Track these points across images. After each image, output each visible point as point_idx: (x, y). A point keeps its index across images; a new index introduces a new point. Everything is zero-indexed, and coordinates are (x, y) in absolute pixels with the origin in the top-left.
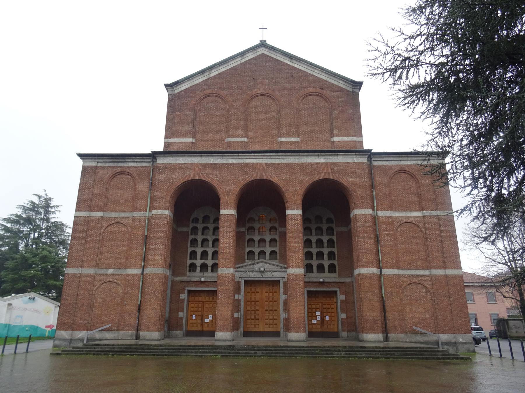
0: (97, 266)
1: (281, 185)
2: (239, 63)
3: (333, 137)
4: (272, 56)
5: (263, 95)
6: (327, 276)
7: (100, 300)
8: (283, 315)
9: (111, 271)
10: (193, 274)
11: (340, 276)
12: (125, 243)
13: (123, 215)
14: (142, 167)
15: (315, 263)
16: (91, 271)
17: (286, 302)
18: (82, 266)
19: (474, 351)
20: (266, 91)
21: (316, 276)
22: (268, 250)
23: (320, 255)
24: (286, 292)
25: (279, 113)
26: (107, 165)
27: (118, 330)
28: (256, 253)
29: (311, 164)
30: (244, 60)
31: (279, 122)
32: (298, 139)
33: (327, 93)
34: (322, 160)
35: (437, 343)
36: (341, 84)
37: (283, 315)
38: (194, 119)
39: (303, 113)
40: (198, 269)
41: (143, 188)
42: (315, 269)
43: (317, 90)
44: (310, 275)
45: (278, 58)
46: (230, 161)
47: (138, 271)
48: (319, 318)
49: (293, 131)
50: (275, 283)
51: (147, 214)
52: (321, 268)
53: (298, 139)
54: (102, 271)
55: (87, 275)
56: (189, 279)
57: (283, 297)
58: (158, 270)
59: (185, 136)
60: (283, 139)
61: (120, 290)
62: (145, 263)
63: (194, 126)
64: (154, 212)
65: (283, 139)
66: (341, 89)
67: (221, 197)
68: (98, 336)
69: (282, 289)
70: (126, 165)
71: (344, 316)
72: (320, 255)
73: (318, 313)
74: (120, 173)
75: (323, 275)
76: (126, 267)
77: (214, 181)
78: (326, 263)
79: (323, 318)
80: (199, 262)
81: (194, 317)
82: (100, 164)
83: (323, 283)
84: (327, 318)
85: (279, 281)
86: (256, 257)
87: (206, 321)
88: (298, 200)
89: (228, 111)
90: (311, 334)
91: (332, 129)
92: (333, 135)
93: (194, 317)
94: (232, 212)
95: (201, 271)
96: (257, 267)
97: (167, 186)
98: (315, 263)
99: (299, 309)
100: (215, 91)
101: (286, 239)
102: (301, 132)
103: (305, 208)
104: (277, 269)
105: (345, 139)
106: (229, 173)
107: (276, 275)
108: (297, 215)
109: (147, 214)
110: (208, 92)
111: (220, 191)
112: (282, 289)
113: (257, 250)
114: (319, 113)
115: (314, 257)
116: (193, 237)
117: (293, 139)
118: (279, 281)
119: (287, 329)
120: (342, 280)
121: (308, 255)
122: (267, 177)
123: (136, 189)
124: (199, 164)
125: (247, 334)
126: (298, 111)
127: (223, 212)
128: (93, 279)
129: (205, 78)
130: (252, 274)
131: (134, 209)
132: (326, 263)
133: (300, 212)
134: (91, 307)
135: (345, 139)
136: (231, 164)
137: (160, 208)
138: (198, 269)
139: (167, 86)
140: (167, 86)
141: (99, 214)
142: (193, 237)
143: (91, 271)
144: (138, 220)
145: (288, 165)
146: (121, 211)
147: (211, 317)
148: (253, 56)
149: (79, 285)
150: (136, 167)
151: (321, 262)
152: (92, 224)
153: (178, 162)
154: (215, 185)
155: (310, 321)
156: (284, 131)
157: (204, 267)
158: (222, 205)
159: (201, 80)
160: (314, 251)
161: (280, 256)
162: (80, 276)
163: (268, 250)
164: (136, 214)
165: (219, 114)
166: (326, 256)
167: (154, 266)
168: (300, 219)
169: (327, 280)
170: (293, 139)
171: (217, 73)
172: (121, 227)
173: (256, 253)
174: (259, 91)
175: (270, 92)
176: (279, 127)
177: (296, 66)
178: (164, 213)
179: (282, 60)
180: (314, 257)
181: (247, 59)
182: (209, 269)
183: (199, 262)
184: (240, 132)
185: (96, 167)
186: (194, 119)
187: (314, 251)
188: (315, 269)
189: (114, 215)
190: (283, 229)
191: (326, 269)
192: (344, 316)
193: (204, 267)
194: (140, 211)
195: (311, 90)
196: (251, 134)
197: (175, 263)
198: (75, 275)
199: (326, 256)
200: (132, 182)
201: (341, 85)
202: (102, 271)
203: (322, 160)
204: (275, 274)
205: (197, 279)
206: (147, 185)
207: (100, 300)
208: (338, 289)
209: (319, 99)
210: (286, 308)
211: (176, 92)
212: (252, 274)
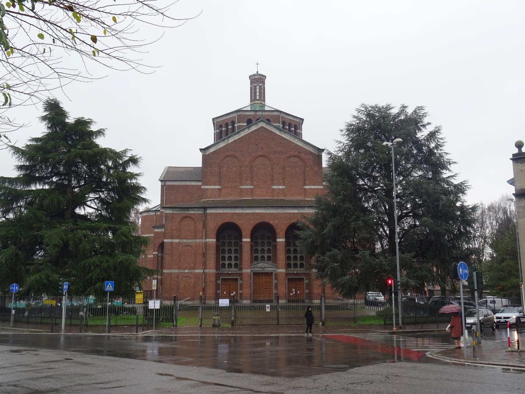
0: (179, 269)
1: (274, 225)
2: (247, 133)
3: (305, 185)
4: (268, 128)
5: (261, 156)
6: (299, 270)
7: (182, 286)
8: (275, 291)
9: (187, 271)
10: (225, 269)
11: (306, 270)
12: (193, 256)
13: (190, 241)
14: (198, 214)
15: (292, 262)
16: (177, 271)
17: (276, 284)
18: (172, 269)
19: (364, 308)
20: (264, 154)
21: (293, 270)
22: (266, 255)
23: (295, 258)
24: (276, 279)
25: (272, 169)
26: (178, 212)
27: (193, 300)
28: (259, 257)
29: (290, 213)
30: (250, 131)
31: (273, 175)
32: (284, 187)
33: (303, 155)
34: (296, 211)
35: (347, 304)
36: (311, 150)
37: (275, 291)
38: (220, 173)
39: (287, 169)
40: (227, 266)
41: (200, 226)
42: (292, 266)
43: (296, 153)
44: (289, 269)
45: (272, 130)
46: (247, 212)
47: (201, 271)
48: (294, 293)
49: (281, 181)
50: (270, 274)
51: (204, 241)
52: (295, 265)
53: (284, 187)
54: (182, 271)
55: (175, 273)
56: (222, 272)
57: (275, 282)
58: (211, 271)
59: (214, 184)
60: (275, 187)
61: (192, 281)
62: (205, 267)
63: (220, 178)
64: (208, 240)
65: (275, 187)
66: (311, 153)
67: (243, 231)
68: (184, 303)
69: (274, 278)
70: (189, 212)
71: (307, 291)
72: (295, 258)
73: (294, 290)
74: (186, 217)
75: (297, 269)
76: (195, 269)
77: (239, 223)
78: (299, 263)
79: (296, 292)
80: (227, 262)
81: (225, 293)
82: (174, 212)
83: (297, 273)
84: (298, 292)
85: (272, 273)
86: (259, 260)
87: (232, 295)
88: (283, 233)
89: (241, 167)
90: (289, 301)
91: (305, 180)
92: (305, 185)
93: (225, 293)
94: (249, 240)
95: (228, 268)
96: (260, 265)
97: (213, 226)
98: (292, 262)
99: (282, 290)
100: (232, 153)
101: (276, 256)
102: (286, 182)
103: (287, 237)
104: (271, 266)
105: (312, 187)
106: (247, 217)
107: (270, 270)
108: (282, 242)
109: (204, 241)
110: (228, 154)
111: (242, 229)
112: (274, 278)
113: (260, 255)
114: (297, 169)
115: (292, 259)
116: (223, 248)
117: (281, 187)
118: (272, 273)
119: (242, 298)
120: (307, 272)
121: (288, 258)
122: (267, 221)
123: (195, 226)
124: (230, 213)
125: (255, 301)
126: (284, 168)
127: (244, 240)
128: (178, 275)
129: (225, 144)
130: (257, 269)
131: (195, 238)
132: (299, 263)
133: (284, 240)
134: (179, 289)
135: (312, 187)
136: (248, 213)
137: (211, 238)
138: (227, 266)
139: (201, 150)
140: (201, 150)
141: (177, 241)
142: (223, 248)
143: (177, 271)
144: (198, 244)
145: (278, 214)
146: (189, 239)
147: (234, 293)
148: (256, 128)
149: (171, 278)
150: (195, 214)
151: (296, 262)
152: (174, 246)
153: (218, 212)
154: (239, 225)
155: (289, 294)
156: (275, 182)
157: (230, 265)
158: (243, 236)
159: (223, 145)
160: (292, 256)
161: (272, 259)
162: (171, 274)
163: (266, 255)
164: (197, 241)
165: (235, 169)
166: (298, 259)
167: (210, 268)
168: (284, 244)
169: (298, 272)
170: (281, 187)
171: (233, 140)
172: (190, 248)
173: (259, 257)
174: (260, 154)
175: (267, 154)
176: (273, 179)
177: (283, 136)
178: (212, 240)
179: (274, 131)
180: (292, 259)
181: (252, 130)
182: (233, 266)
183: (227, 262)
184: (249, 182)
185: (172, 214)
186: (220, 173)
187: (292, 256)
188: (292, 266)
189: (185, 241)
190: (275, 243)
191: (299, 266)
192: (307, 291)
193: (230, 265)
194: (199, 239)
195: (292, 153)
196: (255, 183)
197: (219, 266)
198: (169, 273)
199: (298, 259)
200: (193, 222)
201: (311, 150)
202: (182, 271)
203: (296, 211)
204: (270, 269)
205: (227, 272)
206: (202, 224)
207: (182, 286)
208: (304, 277)
209: (297, 159)
210: (276, 288)
211: (207, 153)
212: (257, 269)
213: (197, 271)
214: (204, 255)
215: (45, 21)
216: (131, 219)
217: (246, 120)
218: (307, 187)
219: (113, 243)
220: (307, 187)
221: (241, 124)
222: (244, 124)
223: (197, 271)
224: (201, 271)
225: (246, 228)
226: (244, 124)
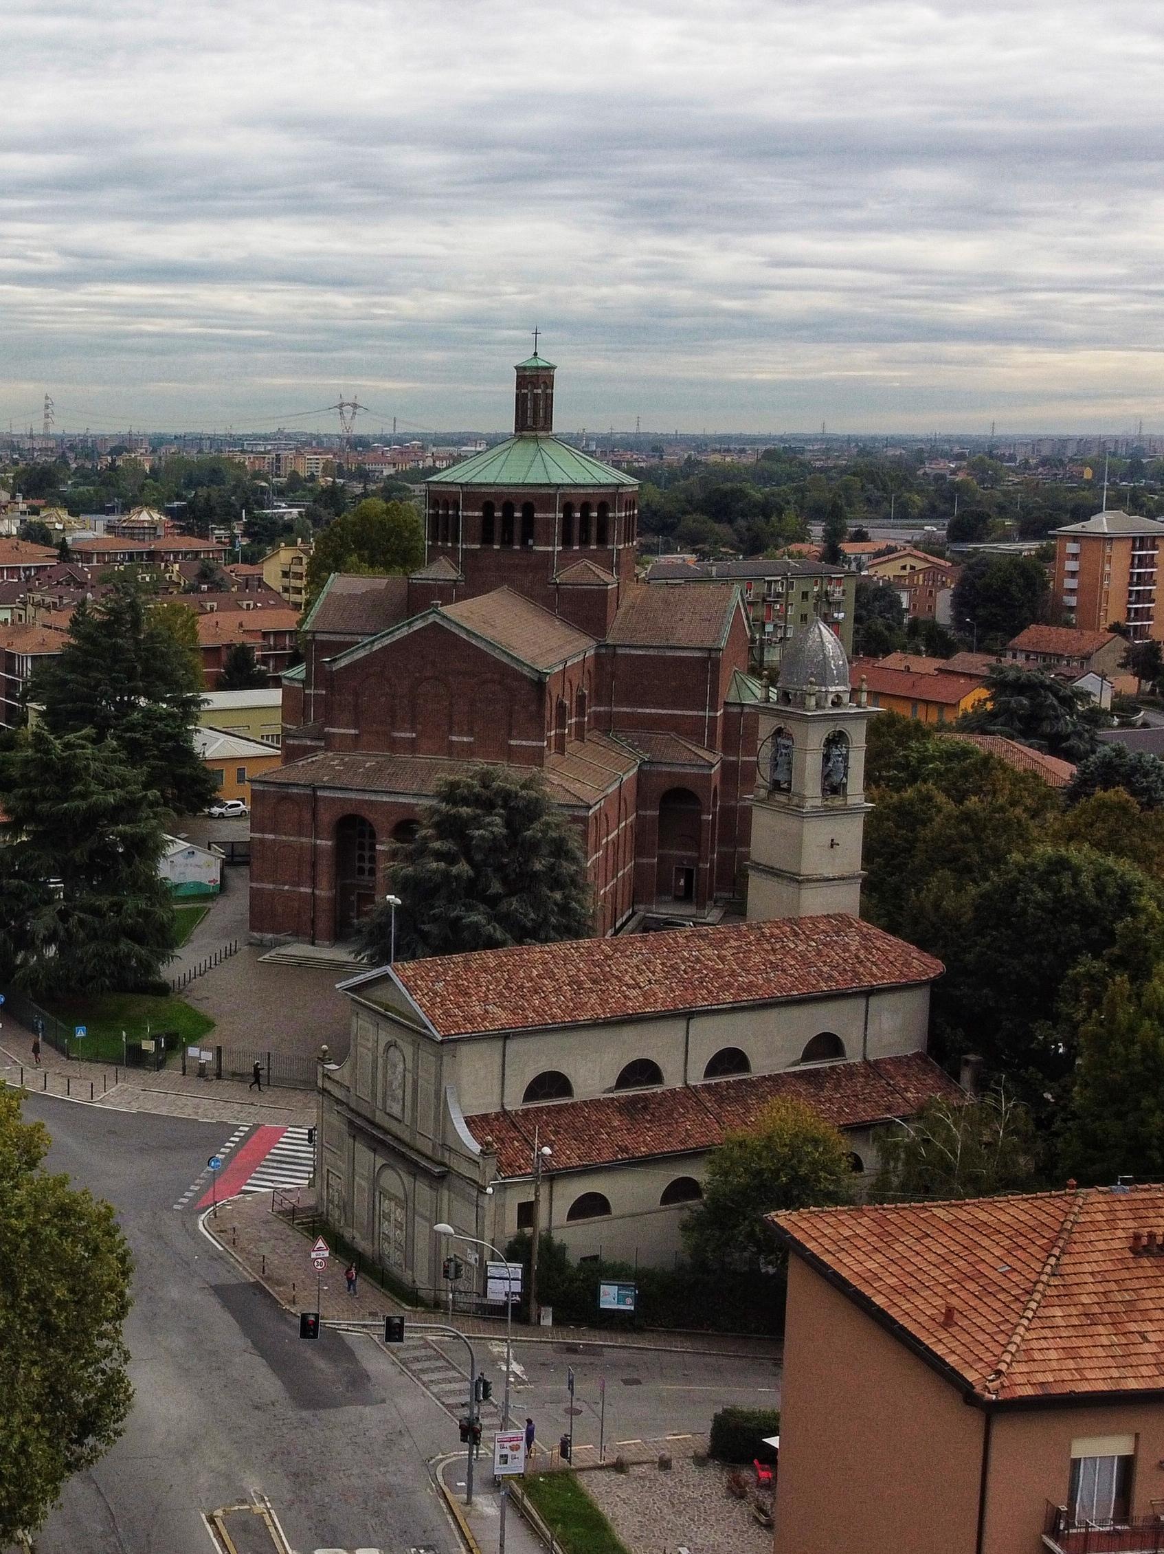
16: (271, 886)
32: (472, 739)
41: (307, 816)
47: (309, 890)
60: (454, 738)
61: (296, 904)
64: (318, 842)
65: (454, 738)
76: (299, 885)
77: (371, 817)
97: (327, 817)
102: (476, 730)
114: (498, 707)
128: (272, 893)
131: (300, 834)
141: (272, 837)
143: (271, 886)
164: (304, 840)
178: (325, 843)
213: (302, 890)
214: (314, 865)
215: (56, 629)
216: (162, 874)
217: (481, 504)
218: (513, 742)
219: (322, 542)
220: (513, 742)
221: (470, 514)
222: (476, 514)
223: (302, 890)
224: (309, 890)
225: (383, 824)
226: (476, 514)
